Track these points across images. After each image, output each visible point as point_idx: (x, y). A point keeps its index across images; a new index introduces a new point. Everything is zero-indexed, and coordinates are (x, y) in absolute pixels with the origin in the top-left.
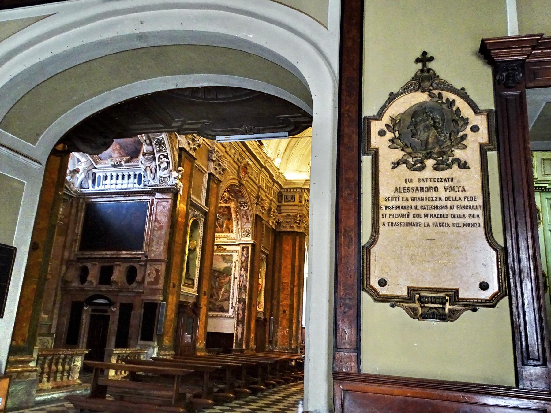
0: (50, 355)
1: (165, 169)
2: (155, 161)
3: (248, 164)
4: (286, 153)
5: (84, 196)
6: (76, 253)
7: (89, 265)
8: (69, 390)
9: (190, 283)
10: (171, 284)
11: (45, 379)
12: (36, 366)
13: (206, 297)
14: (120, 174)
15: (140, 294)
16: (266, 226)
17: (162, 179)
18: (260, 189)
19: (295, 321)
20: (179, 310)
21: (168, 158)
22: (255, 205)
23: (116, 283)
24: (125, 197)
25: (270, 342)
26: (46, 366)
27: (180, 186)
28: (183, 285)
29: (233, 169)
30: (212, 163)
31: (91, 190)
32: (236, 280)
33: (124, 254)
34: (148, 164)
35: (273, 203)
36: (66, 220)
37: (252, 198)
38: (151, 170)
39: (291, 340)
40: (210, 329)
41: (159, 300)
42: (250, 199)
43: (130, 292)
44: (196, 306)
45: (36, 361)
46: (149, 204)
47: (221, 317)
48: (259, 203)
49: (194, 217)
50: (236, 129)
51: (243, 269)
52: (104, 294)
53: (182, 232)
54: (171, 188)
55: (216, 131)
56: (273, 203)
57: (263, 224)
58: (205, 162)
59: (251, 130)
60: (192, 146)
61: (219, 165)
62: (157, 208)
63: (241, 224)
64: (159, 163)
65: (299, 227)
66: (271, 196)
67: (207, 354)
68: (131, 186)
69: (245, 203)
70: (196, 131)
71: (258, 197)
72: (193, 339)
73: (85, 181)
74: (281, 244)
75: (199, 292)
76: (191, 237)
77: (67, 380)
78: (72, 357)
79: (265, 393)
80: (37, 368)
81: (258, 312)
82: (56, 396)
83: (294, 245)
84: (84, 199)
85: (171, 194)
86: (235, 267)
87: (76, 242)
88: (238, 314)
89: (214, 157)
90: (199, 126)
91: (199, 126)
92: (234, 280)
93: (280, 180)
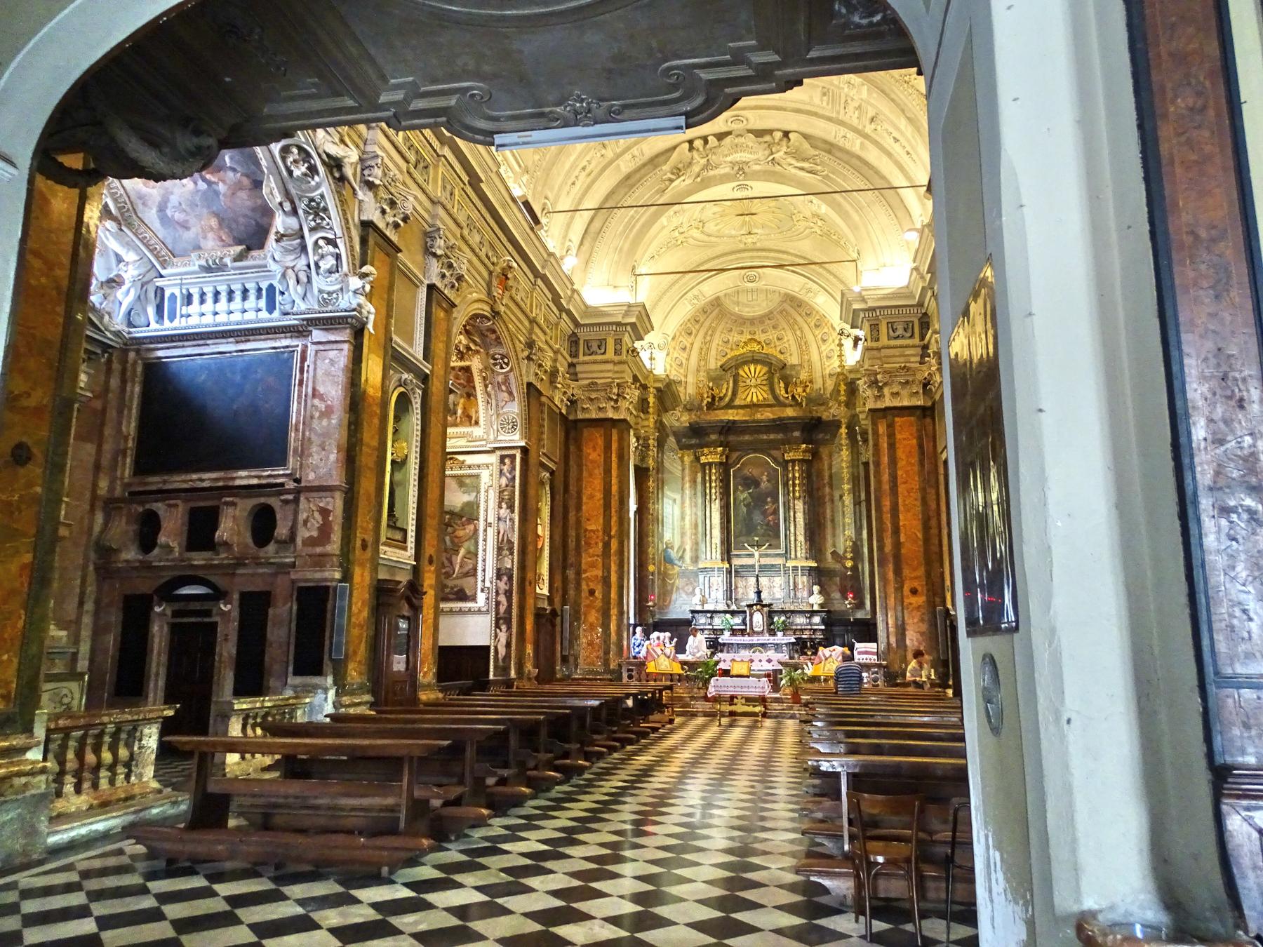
0: (77, 728)
1: (330, 272)
2: (307, 254)
3: (511, 267)
4: (584, 248)
5: (137, 344)
6: (126, 481)
7: (160, 507)
8: (132, 809)
9: (398, 536)
10: (358, 543)
11: (69, 788)
12: (45, 759)
13: (433, 568)
14: (222, 288)
15: (284, 569)
16: (549, 407)
17: (326, 296)
18: (535, 325)
19: (614, 612)
20: (378, 598)
21: (336, 246)
22: (526, 361)
23: (227, 545)
24: (237, 342)
25: (565, 660)
26: (70, 755)
27: (368, 312)
28: (384, 544)
29: (479, 278)
30: (434, 260)
31: (155, 329)
32: (489, 528)
33: (244, 477)
34: (289, 260)
35: (560, 357)
36: (98, 404)
37: (520, 346)
38: (297, 276)
39: (607, 652)
40: (444, 641)
41: (333, 580)
42: (515, 348)
43: (259, 564)
44: (414, 588)
45: (42, 747)
46: (297, 358)
47: (461, 612)
48: (534, 357)
49: (400, 385)
50: (547, 110)
51: (504, 505)
52: (200, 573)
53: (376, 421)
54: (346, 317)
55: (496, 119)
56: (560, 357)
57: (542, 404)
58: (419, 257)
59: (589, 111)
60: (391, 220)
61: (450, 266)
62: (315, 364)
63: (497, 405)
64: (316, 258)
65: (616, 409)
66: (556, 344)
67: (441, 695)
68: (251, 315)
69: (503, 357)
70: (444, 119)
71: (530, 345)
72: (411, 665)
73: (138, 307)
74: (580, 449)
75: (417, 557)
76: (396, 431)
77: (125, 784)
78: (135, 729)
79: (586, 776)
80: (48, 764)
81: (537, 597)
82: (100, 826)
83: (608, 448)
84: (138, 351)
85: (348, 331)
86: (486, 501)
87: (125, 456)
88: (498, 604)
89: (439, 247)
90: (452, 101)
91: (452, 101)
92: (485, 530)
93: (574, 307)
